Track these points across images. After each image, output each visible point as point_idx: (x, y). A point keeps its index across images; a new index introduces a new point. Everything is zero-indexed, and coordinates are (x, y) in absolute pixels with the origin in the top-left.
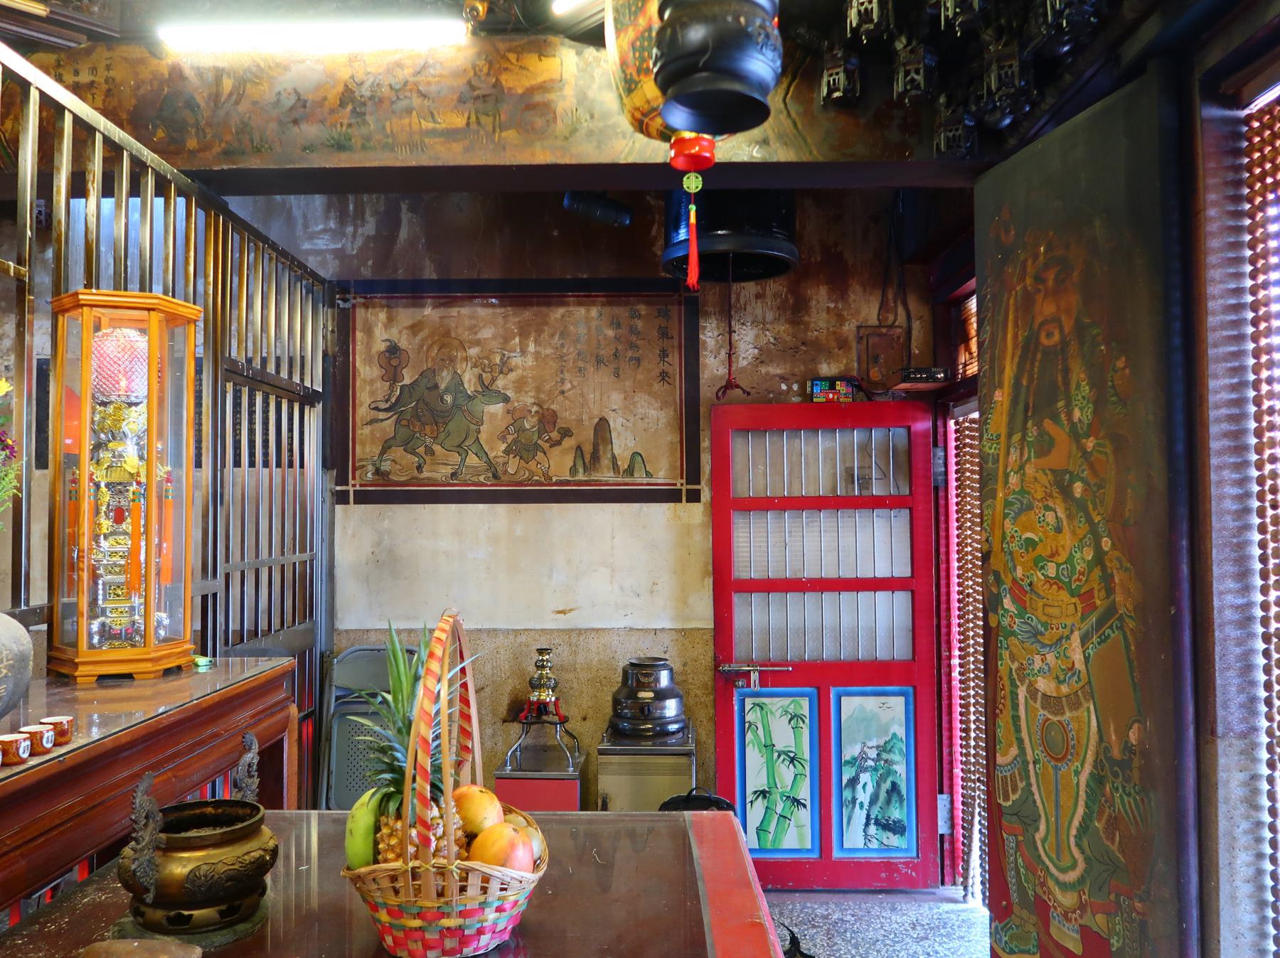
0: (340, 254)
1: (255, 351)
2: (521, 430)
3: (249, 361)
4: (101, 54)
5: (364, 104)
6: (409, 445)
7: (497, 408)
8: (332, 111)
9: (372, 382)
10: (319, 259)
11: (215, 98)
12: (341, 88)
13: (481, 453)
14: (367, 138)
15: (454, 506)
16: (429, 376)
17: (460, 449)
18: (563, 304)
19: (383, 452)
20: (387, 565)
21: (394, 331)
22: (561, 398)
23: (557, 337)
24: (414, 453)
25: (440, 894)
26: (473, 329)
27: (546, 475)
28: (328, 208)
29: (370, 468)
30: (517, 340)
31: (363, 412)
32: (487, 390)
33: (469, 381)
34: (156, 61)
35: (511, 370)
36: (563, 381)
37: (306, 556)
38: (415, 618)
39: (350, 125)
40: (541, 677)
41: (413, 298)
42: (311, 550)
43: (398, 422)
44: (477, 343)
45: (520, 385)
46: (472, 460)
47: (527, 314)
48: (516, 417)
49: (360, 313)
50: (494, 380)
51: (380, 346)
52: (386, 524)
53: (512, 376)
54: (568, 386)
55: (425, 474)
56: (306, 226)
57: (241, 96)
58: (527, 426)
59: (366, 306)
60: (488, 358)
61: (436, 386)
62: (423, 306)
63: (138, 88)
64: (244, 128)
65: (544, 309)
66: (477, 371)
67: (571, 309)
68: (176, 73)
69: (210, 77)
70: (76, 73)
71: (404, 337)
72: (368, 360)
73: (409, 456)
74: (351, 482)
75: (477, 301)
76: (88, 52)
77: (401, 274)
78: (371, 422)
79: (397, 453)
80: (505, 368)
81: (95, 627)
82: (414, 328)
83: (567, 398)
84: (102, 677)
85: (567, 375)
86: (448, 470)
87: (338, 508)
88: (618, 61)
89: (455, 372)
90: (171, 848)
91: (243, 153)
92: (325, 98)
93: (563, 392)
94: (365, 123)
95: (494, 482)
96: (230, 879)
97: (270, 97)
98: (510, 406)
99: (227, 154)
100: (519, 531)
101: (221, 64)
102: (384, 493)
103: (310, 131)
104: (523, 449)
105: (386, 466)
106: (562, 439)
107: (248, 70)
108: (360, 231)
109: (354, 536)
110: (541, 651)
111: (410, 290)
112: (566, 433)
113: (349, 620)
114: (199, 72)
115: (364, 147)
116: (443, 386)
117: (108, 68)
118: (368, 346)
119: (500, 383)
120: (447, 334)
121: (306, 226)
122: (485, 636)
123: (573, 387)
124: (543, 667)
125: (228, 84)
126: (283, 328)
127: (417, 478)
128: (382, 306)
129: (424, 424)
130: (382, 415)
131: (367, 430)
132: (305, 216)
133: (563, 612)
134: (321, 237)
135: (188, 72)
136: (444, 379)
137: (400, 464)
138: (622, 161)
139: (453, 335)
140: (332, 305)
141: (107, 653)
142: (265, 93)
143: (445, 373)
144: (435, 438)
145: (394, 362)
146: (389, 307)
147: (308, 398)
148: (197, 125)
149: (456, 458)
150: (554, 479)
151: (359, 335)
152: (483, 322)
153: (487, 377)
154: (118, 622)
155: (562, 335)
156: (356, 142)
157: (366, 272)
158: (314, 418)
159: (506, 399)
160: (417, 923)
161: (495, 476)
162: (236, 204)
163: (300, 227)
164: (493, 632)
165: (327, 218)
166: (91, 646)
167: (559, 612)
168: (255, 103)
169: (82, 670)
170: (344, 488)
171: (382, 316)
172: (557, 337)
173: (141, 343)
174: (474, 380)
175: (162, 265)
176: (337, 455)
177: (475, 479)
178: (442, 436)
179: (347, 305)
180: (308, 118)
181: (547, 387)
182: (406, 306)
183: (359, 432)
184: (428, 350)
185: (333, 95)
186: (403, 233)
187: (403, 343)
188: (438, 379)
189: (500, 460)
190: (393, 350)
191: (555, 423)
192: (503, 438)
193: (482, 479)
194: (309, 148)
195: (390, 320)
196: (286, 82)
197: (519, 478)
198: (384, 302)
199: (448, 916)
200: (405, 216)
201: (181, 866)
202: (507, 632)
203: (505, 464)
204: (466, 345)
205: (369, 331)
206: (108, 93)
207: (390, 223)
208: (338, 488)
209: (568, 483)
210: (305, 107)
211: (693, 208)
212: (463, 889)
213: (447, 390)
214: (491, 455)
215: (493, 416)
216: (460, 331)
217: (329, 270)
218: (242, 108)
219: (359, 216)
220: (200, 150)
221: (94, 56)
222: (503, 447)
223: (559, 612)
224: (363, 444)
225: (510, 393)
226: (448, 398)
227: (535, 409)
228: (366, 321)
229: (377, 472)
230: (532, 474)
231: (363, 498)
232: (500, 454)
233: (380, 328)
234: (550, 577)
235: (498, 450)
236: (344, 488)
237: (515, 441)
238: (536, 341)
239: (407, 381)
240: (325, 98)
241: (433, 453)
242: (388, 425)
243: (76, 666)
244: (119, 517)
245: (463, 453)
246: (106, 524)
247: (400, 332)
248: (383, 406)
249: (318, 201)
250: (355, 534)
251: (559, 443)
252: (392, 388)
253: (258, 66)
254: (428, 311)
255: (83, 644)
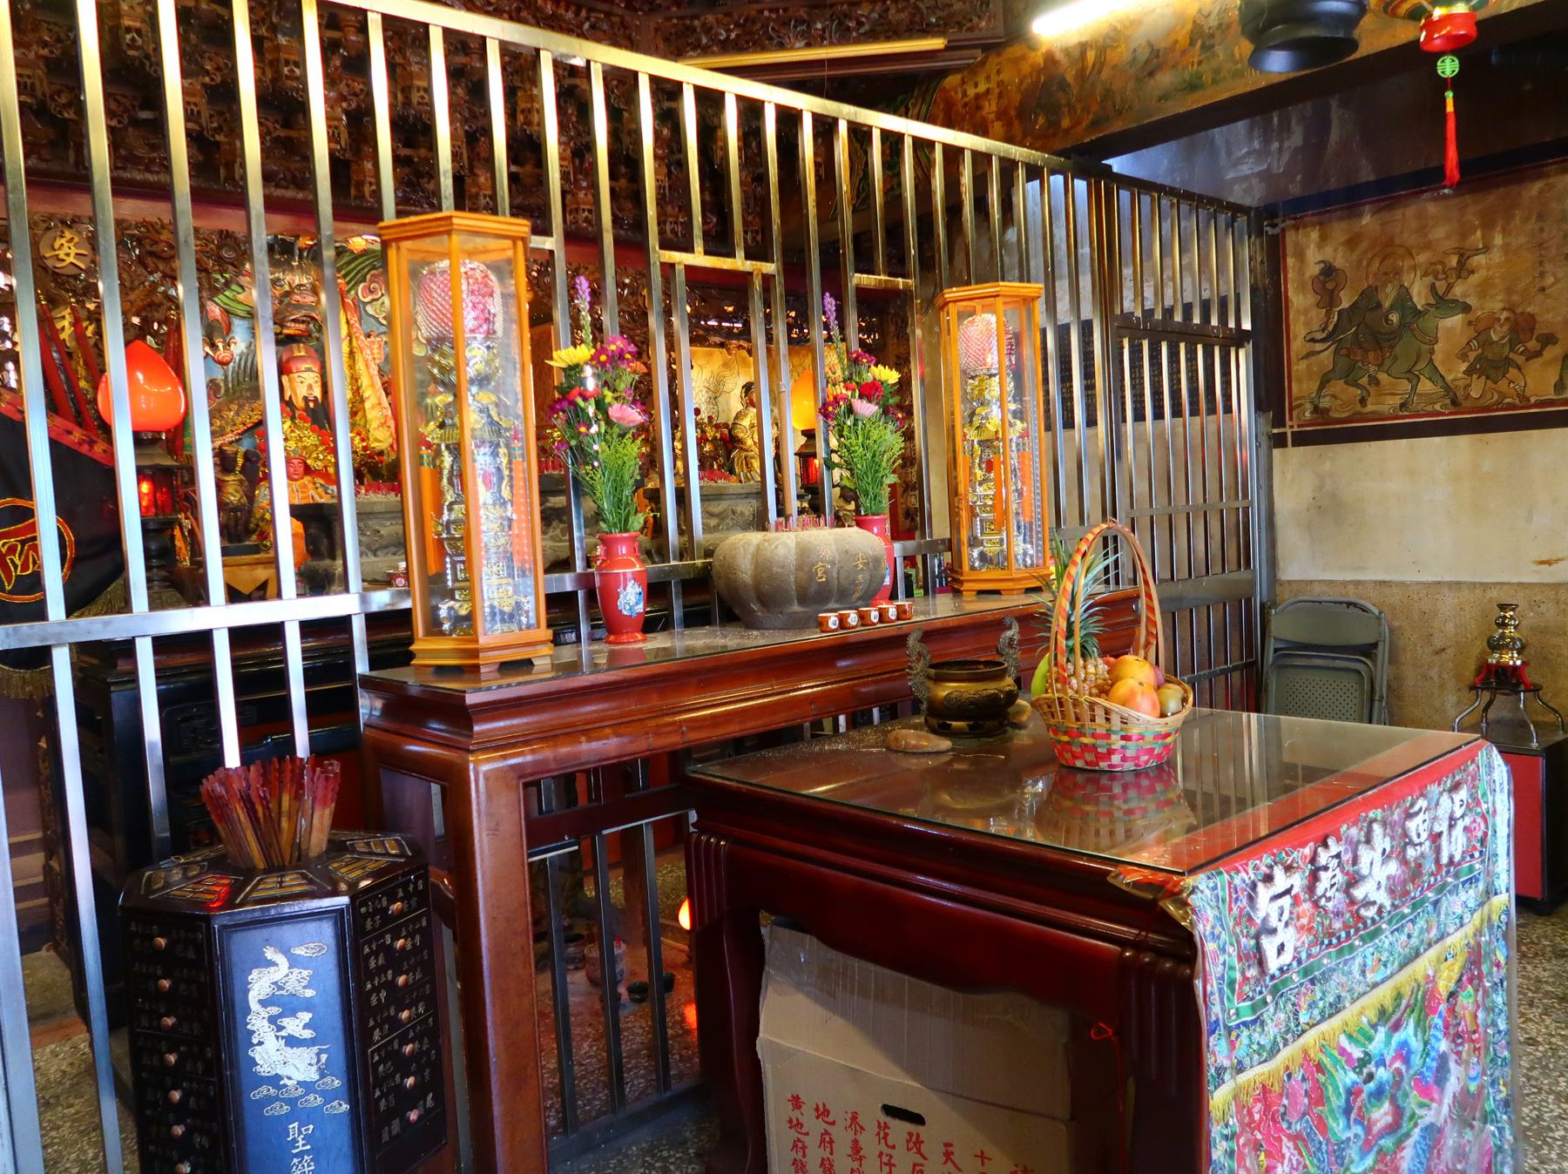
0: (1266, 176)
1: (1175, 300)
2: (1486, 343)
3: (1168, 312)
4: (993, 61)
5: (1212, 36)
6: (1350, 377)
7: (1455, 321)
8: (1183, 52)
9: (1306, 311)
10: (1244, 186)
11: (1081, 75)
12: (1189, 26)
13: (1436, 375)
14: (1217, 71)
15: (1404, 441)
16: (1369, 300)
17: (1412, 376)
18: (1539, 177)
19: (1322, 386)
20: (1330, 510)
21: (1329, 250)
22: (1540, 296)
23: (1533, 220)
24: (1357, 386)
25: (1078, 719)
26: (1423, 230)
27: (1524, 398)
28: (1251, 130)
29: (1309, 406)
30: (1479, 233)
31: (1298, 345)
32: (1443, 303)
33: (1419, 294)
34: (1032, 54)
35: (1473, 272)
36: (1542, 275)
37: (1240, 504)
38: (1363, 569)
39: (1200, 63)
40: (1503, 636)
41: (1348, 208)
42: (1245, 496)
43: (1336, 352)
44: (1428, 246)
45: (1484, 289)
46: (1426, 386)
47: (1491, 199)
48: (1480, 330)
49: (1290, 237)
50: (1450, 287)
51: (1314, 269)
52: (1328, 465)
53: (1474, 279)
54: (1550, 280)
55: (1370, 408)
56: (1229, 154)
57: (1103, 64)
58: (1495, 338)
59: (1296, 228)
60: (1441, 263)
61: (1379, 305)
62: (1360, 215)
63: (1021, 83)
64: (1108, 93)
65: (1515, 188)
66: (1429, 279)
67: (1551, 180)
68: (1050, 58)
69: (1076, 53)
70: (976, 85)
71: (1340, 254)
72: (1301, 288)
73: (1352, 389)
74: (1288, 423)
75: (1425, 196)
76: (983, 63)
77: (1333, 184)
78: (1307, 356)
79: (1338, 386)
80: (1463, 270)
81: (976, 553)
82: (1352, 243)
83: (1549, 296)
84: (980, 592)
85: (1548, 267)
86: (1397, 401)
87: (1276, 452)
88: (575, 361)
89: (1402, 286)
90: (939, 679)
91: (1107, 119)
92: (1176, 42)
93: (1543, 289)
94: (1215, 55)
95: (1453, 409)
96: (971, 703)
97: (1127, 57)
98: (1471, 316)
99: (1095, 124)
100: (1487, 466)
101: (1084, 39)
102: (1327, 432)
103: (1165, 79)
104: (1489, 365)
105: (1325, 403)
106: (1542, 349)
107: (1107, 36)
108: (1286, 144)
109: (1293, 480)
110: (1503, 607)
111: (1348, 199)
112: (1549, 340)
113: (1291, 571)
114: (1067, 51)
115: (1214, 82)
116: (1387, 305)
117: (999, 72)
118: (1301, 271)
119: (1458, 291)
120: (1390, 243)
121: (1229, 154)
122: (1445, 590)
123: (1557, 280)
124: (1504, 625)
125: (1091, 56)
126: (1187, 268)
127: (1359, 413)
128: (1313, 225)
129: (1366, 351)
130: (1319, 347)
131: (1303, 365)
132: (1228, 142)
133: (1549, 563)
134: (1244, 164)
135: (1059, 56)
136: (1388, 296)
137: (1341, 399)
138: (1504, 11)
139: (1397, 242)
140: (1260, 234)
141: (986, 573)
142: (1122, 54)
143: (1388, 289)
144: (1380, 366)
145: (1330, 286)
146: (1321, 224)
147: (1239, 338)
148: (1068, 104)
149: (1405, 386)
150: (1533, 400)
151: (1290, 261)
152: (1432, 222)
153: (1441, 286)
154: (991, 549)
155: (1540, 217)
156: (1207, 78)
157: (1295, 190)
158: (1243, 361)
159: (1467, 308)
160: (1066, 739)
161: (1454, 403)
162: (1117, 164)
163: (1223, 154)
164: (1456, 586)
165: (1251, 139)
166: (973, 568)
167: (1542, 563)
168: (1114, 67)
169: (966, 586)
170: (1281, 430)
171: (1315, 235)
172: (1533, 220)
173: (993, 318)
174: (1425, 291)
175: (1040, 241)
176: (1271, 396)
177: (1429, 408)
178: (1388, 362)
179: (1277, 231)
180: (1160, 67)
181: (1521, 286)
182: (1341, 219)
183: (1294, 368)
184: (1368, 265)
185: (1183, 36)
186: (1335, 135)
187: (1339, 262)
188: (1381, 296)
189: (1461, 383)
190: (1328, 271)
191: (1532, 330)
192: (1463, 357)
193: (1437, 407)
194: (1164, 97)
195: (1324, 238)
196: (1139, 38)
197: (1482, 403)
198: (1315, 219)
199: (1084, 735)
200: (1336, 113)
201: (945, 690)
202: (1473, 585)
203: (1467, 386)
204: (1414, 251)
205: (1300, 255)
206: (1000, 96)
207: (1318, 129)
208: (1275, 431)
209: (1551, 403)
210: (1157, 57)
211: (1449, 95)
212: (1093, 720)
213: (1392, 308)
214: (1449, 378)
215: (1450, 331)
216: (1405, 235)
217: (1247, 194)
218: (1105, 75)
219: (1285, 127)
220: (1072, 127)
221: (988, 66)
222: (1464, 366)
223: (1542, 563)
224: (1299, 381)
225: (1471, 301)
226: (1394, 317)
227: (1504, 315)
228: (1297, 244)
229: (1316, 409)
230: (1503, 395)
231: (1302, 439)
232: (1460, 375)
233: (1311, 251)
234: (1529, 519)
235: (1456, 372)
236: (1281, 430)
237: (1479, 359)
238: (1505, 231)
239: (1345, 304)
240: (1176, 42)
241: (1377, 383)
242: (1326, 357)
243: (962, 582)
244: (990, 466)
245: (1412, 376)
246: (979, 473)
247: (1335, 250)
248: (1320, 336)
249: (1241, 126)
250: (1297, 477)
251: (1538, 354)
252: (1328, 315)
253: (1115, 29)
254: (1366, 220)
255: (966, 568)
